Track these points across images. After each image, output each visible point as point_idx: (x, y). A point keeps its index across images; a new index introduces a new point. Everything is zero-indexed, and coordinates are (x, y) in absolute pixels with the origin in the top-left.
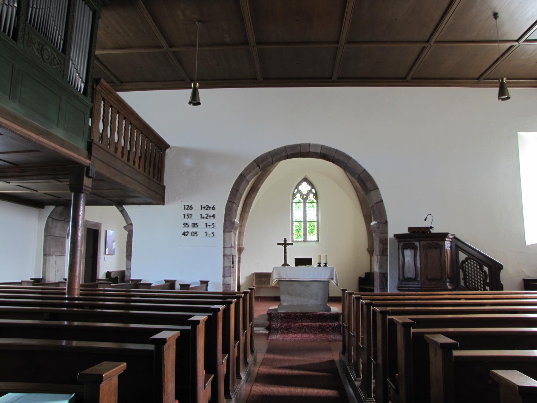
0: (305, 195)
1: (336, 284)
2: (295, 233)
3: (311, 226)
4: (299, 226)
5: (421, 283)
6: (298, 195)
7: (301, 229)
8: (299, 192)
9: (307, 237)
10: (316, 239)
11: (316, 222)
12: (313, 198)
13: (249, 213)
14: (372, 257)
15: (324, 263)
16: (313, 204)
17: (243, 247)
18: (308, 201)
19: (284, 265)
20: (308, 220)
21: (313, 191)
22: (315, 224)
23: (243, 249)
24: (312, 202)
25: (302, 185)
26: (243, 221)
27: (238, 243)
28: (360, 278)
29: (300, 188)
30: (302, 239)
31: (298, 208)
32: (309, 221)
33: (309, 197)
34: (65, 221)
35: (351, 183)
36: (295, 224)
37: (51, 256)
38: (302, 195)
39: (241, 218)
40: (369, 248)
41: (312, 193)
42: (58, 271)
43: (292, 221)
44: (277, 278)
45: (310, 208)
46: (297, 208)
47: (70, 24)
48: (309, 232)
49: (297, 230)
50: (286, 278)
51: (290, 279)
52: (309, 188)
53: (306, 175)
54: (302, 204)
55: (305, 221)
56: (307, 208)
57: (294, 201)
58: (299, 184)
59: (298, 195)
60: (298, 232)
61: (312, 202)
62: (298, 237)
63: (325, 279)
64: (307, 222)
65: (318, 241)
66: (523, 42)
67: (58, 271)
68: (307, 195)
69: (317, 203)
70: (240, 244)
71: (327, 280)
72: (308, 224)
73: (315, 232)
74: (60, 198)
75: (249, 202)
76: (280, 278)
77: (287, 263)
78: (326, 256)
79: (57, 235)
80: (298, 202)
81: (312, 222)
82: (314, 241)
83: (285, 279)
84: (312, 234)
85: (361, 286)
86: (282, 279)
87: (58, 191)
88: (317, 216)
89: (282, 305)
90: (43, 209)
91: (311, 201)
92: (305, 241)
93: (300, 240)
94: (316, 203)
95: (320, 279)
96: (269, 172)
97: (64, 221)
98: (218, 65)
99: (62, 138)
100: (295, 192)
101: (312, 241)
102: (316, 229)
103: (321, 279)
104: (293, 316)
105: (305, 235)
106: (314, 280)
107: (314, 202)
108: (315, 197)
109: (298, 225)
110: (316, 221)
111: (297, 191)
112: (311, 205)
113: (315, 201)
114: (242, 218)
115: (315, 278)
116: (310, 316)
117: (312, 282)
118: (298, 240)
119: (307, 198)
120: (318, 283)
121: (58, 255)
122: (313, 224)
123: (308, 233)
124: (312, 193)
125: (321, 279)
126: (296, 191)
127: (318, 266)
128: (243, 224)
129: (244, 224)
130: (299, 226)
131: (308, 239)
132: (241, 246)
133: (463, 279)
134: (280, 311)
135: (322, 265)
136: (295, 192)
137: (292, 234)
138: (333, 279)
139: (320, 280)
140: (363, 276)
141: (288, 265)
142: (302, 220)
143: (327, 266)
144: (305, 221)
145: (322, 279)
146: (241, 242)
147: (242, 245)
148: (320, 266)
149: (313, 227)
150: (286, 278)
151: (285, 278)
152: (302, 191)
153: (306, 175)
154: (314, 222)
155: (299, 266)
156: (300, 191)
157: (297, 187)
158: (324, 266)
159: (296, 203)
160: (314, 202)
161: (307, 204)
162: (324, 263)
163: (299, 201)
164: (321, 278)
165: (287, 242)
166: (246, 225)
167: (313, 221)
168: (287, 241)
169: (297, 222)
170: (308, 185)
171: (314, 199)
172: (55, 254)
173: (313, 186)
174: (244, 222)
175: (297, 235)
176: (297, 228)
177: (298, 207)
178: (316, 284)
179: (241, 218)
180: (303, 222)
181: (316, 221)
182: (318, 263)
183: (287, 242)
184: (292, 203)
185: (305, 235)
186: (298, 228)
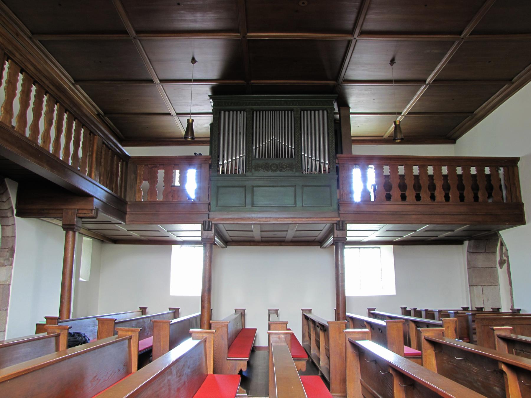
5: (493, 334)
34: (486, 252)
37: (475, 287)
42: (488, 300)
47: (150, 200)
66: (468, 36)
67: (488, 300)
74: (437, 236)
77: (46, 319)
79: (480, 267)
87: (459, 229)
90: (464, 245)
97: (485, 252)
98: (453, 100)
121: (486, 284)
133: (128, 329)
172: (481, 284)
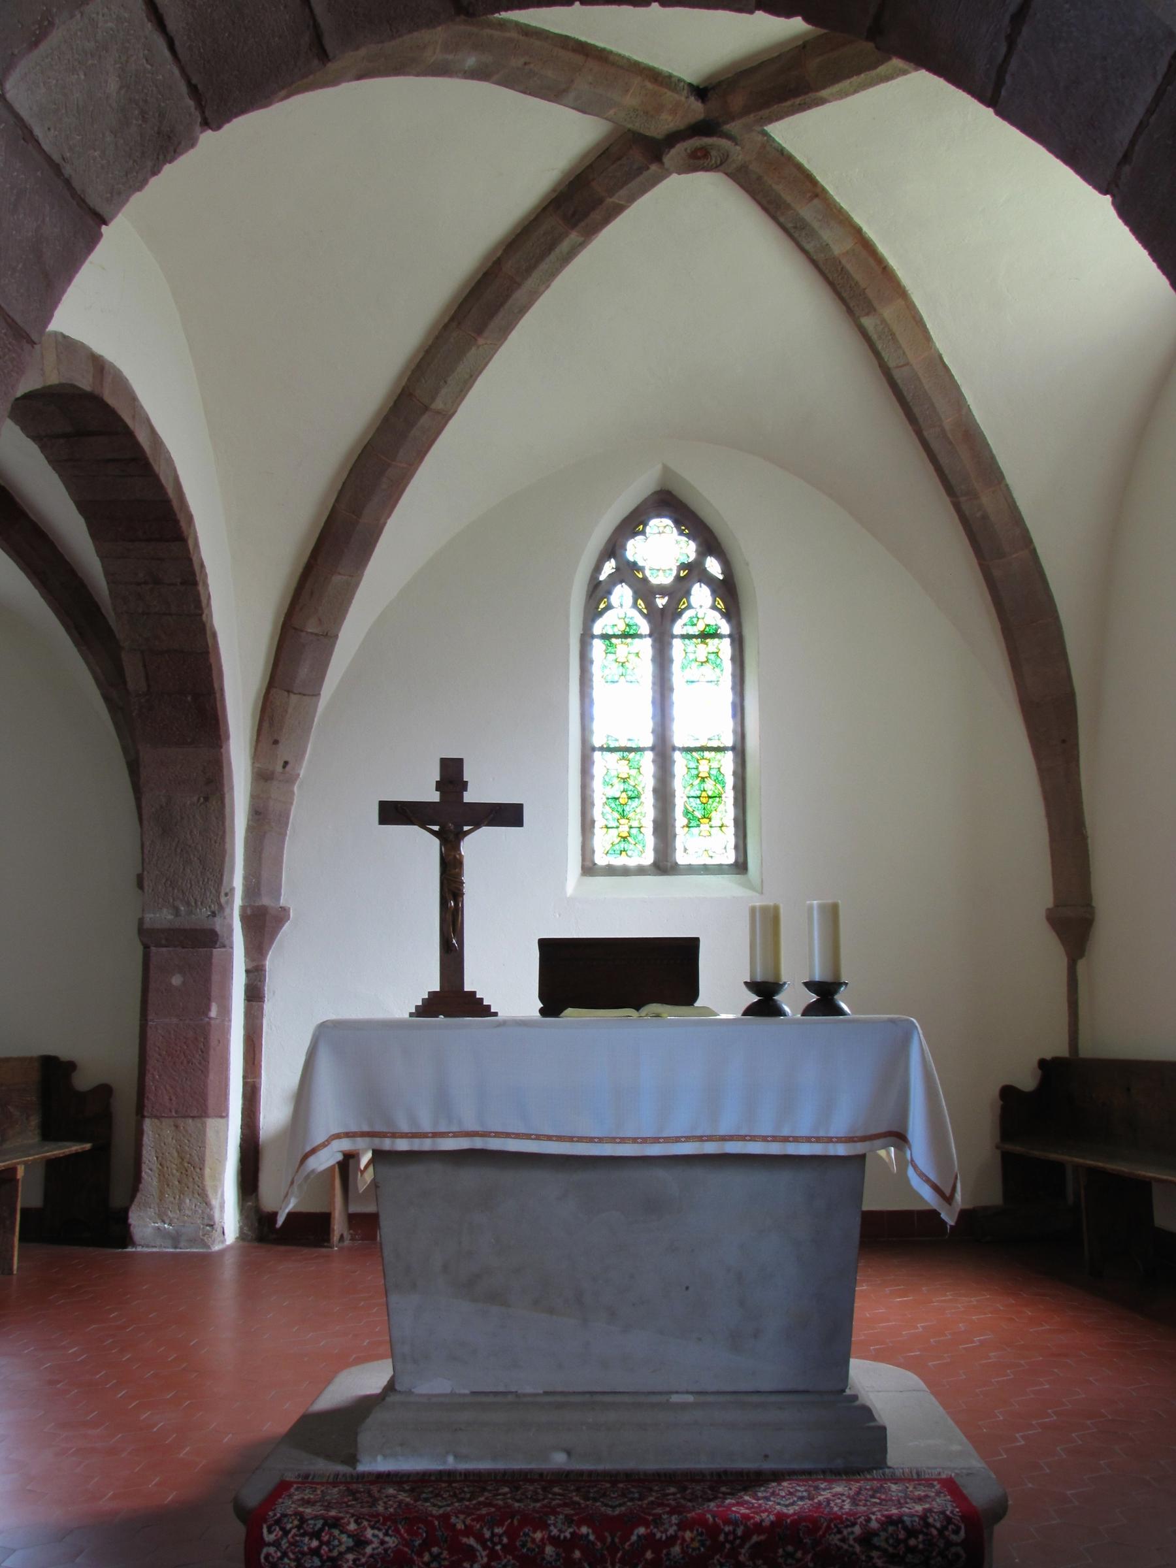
0: (663, 595)
1: (936, 1188)
2: (604, 822)
3: (703, 779)
4: (624, 780)
6: (622, 594)
7: (638, 797)
8: (629, 572)
9: (679, 843)
10: (730, 858)
11: (730, 755)
12: (714, 607)
13: (317, 695)
14: (1081, 965)
15: (810, 985)
16: (713, 643)
17: (282, 902)
18: (678, 628)
19: (431, 1007)
20: (680, 736)
21: (713, 566)
22: (727, 762)
23: (282, 916)
24: (704, 636)
25: (643, 533)
26: (276, 742)
27: (246, 878)
28: (1008, 1093)
29: (635, 549)
30: (648, 859)
31: (621, 670)
32: (689, 750)
33: (689, 607)
35: (947, 500)
36: (602, 763)
38: (644, 591)
39: (266, 725)
40: (1059, 902)
41: (708, 579)
43: (587, 751)
44: (353, 1128)
45: (694, 672)
46: (616, 670)
48: (687, 813)
49: (616, 799)
50: (435, 1135)
51: (478, 1143)
52: (688, 550)
53: (666, 470)
54: (645, 647)
55: (663, 751)
56: (676, 668)
57: (598, 628)
58: (633, 524)
59: (622, 594)
60: (623, 816)
61: (704, 636)
62: (622, 845)
63: (830, 1140)
64: (677, 756)
65: (740, 867)
68: (679, 590)
69: (738, 641)
70: (258, 883)
71: (841, 1150)
72: (680, 762)
73: (726, 811)
75: (312, 627)
76: (378, 1128)
78: (832, 914)
80: (625, 636)
81: (707, 754)
82: (719, 870)
83: (427, 1145)
84: (704, 827)
85: (1009, 1147)
86: (402, 1145)
88: (734, 716)
89: (409, 1393)
91: (701, 627)
92: (664, 865)
93: (632, 862)
94: (727, 642)
95: (775, 1139)
96: (425, 420)
99: (290, 810)
100: (603, 577)
101: (706, 869)
102: (729, 795)
103: (785, 1139)
104: (493, 1556)
105: (664, 829)
106: (710, 1148)
107: (720, 636)
108: (721, 605)
109: (623, 769)
110: (733, 749)
111: (617, 569)
112: (701, 650)
113: (725, 628)
114: (271, 724)
115: (723, 1131)
116: (676, 1550)
117: (699, 1173)
118: (618, 861)
119: (674, 612)
120: (759, 1178)
122: (715, 765)
123: (680, 820)
124: (708, 579)
125: (785, 1139)
126: (609, 567)
127: (751, 1011)
128: (281, 763)
129: (286, 763)
130: (624, 780)
131: (681, 858)
132: (266, 901)
134: (383, 1465)
135: (793, 1000)
136: (603, 577)
137: (587, 826)
138: (899, 1137)
139: (775, 1149)
140: (1027, 1081)
141: (475, 1007)
142: (648, 740)
143: (839, 1012)
144: (663, 751)
145: (796, 1139)
146: (265, 875)
147: (276, 892)
148: (777, 1012)
149: (709, 786)
150: (435, 1135)
151: (427, 1127)
152: (641, 569)
153: (666, 470)
154: (719, 755)
155: (571, 1014)
156: (634, 566)
157: (613, 548)
158: (809, 1011)
159: (605, 637)
160: (715, 635)
161: (677, 646)
162: (810, 985)
163: (628, 625)
164: (785, 1132)
165: (469, 797)
166: (302, 773)
167: (715, 744)
168: (464, 786)
169: (618, 755)
170: (681, 533)
171: (717, 615)
173: (709, 543)
174: (283, 752)
175: (614, 832)
176: (615, 791)
177: (623, 664)
178: (736, 1181)
179: (266, 725)
180: (649, 755)
181: (733, 749)
182: (753, 986)
183: (469, 797)
184: (586, 637)
185: (664, 829)
186: (622, 786)
